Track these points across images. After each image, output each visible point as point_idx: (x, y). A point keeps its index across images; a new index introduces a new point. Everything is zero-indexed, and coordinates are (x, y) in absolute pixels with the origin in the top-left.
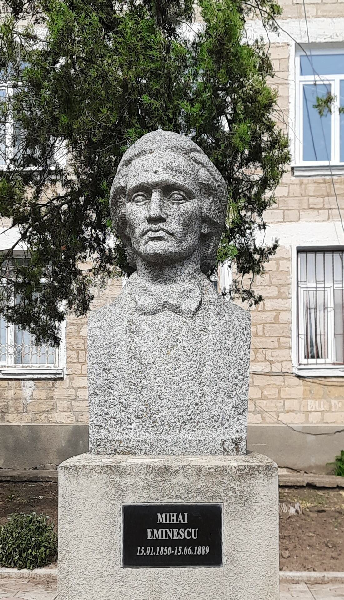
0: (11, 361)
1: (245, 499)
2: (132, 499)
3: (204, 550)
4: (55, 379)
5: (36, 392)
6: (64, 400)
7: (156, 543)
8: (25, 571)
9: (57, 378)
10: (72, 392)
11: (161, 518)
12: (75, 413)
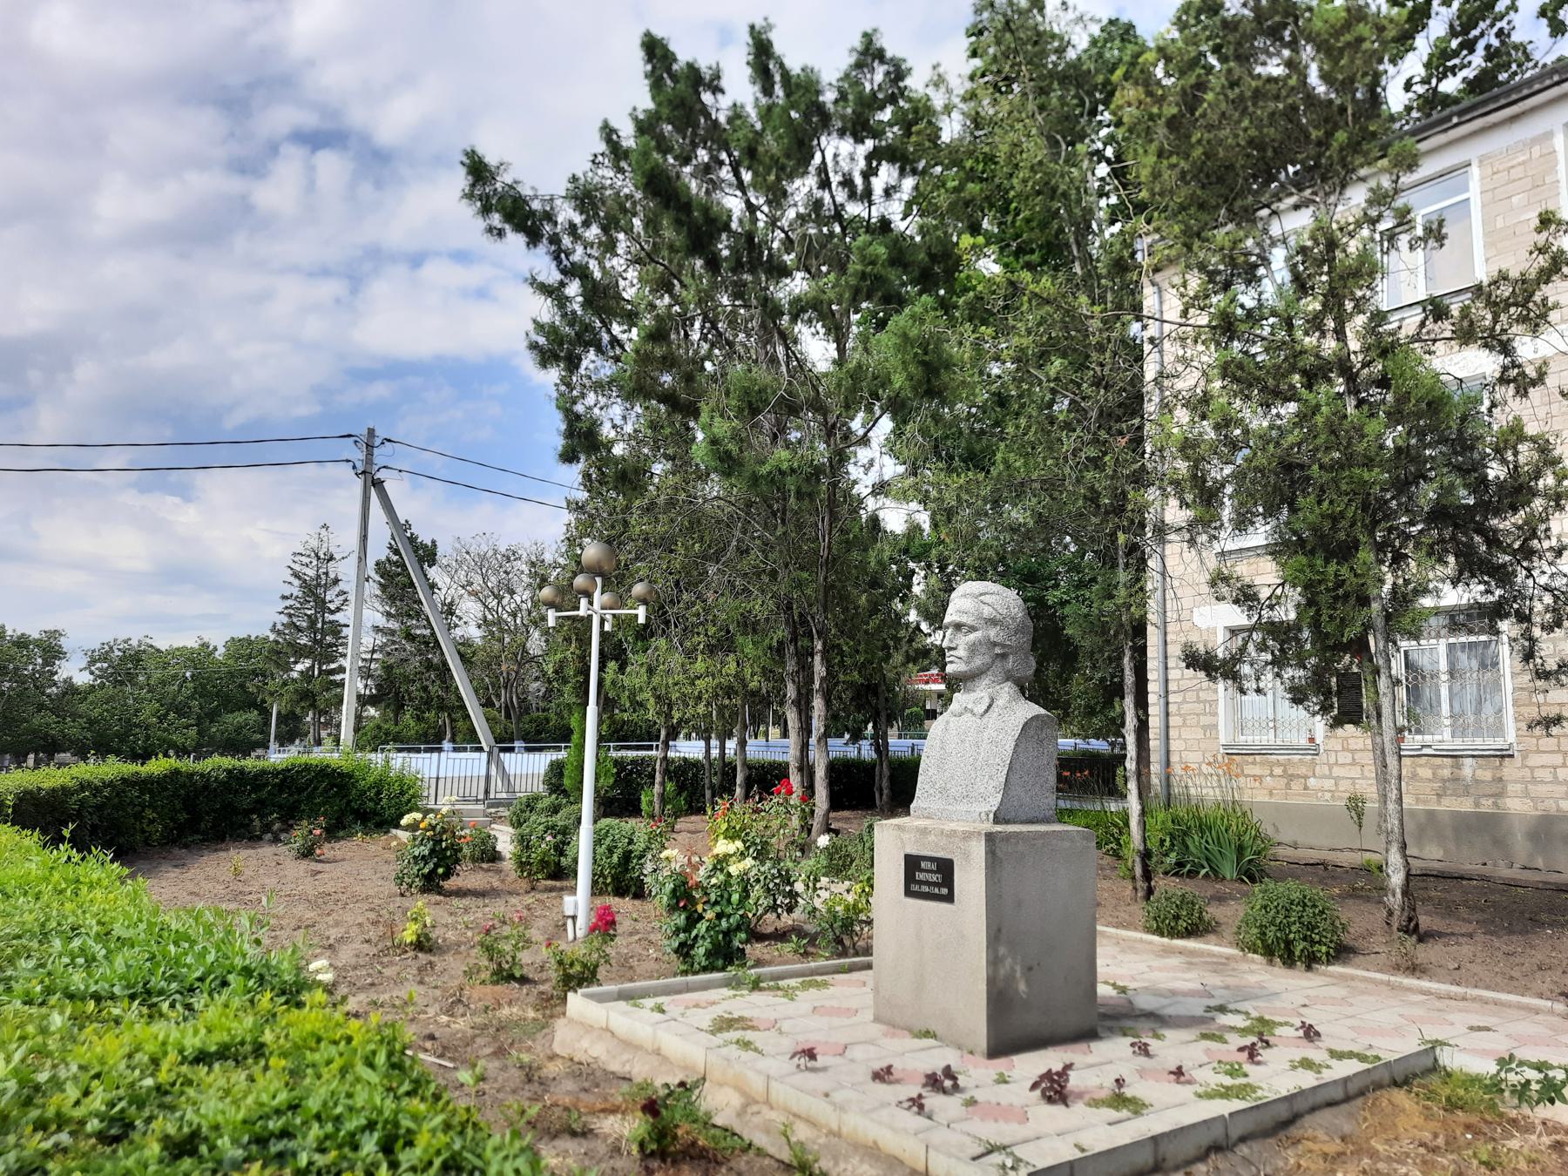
0: (1447, 735)
1: (967, 856)
2: (909, 851)
3: (945, 891)
4: (1503, 757)
5: (1479, 772)
6: (1516, 782)
7: (921, 883)
8: (1166, 940)
9: (1504, 756)
10: (1527, 772)
11: (923, 865)
12: (1532, 799)
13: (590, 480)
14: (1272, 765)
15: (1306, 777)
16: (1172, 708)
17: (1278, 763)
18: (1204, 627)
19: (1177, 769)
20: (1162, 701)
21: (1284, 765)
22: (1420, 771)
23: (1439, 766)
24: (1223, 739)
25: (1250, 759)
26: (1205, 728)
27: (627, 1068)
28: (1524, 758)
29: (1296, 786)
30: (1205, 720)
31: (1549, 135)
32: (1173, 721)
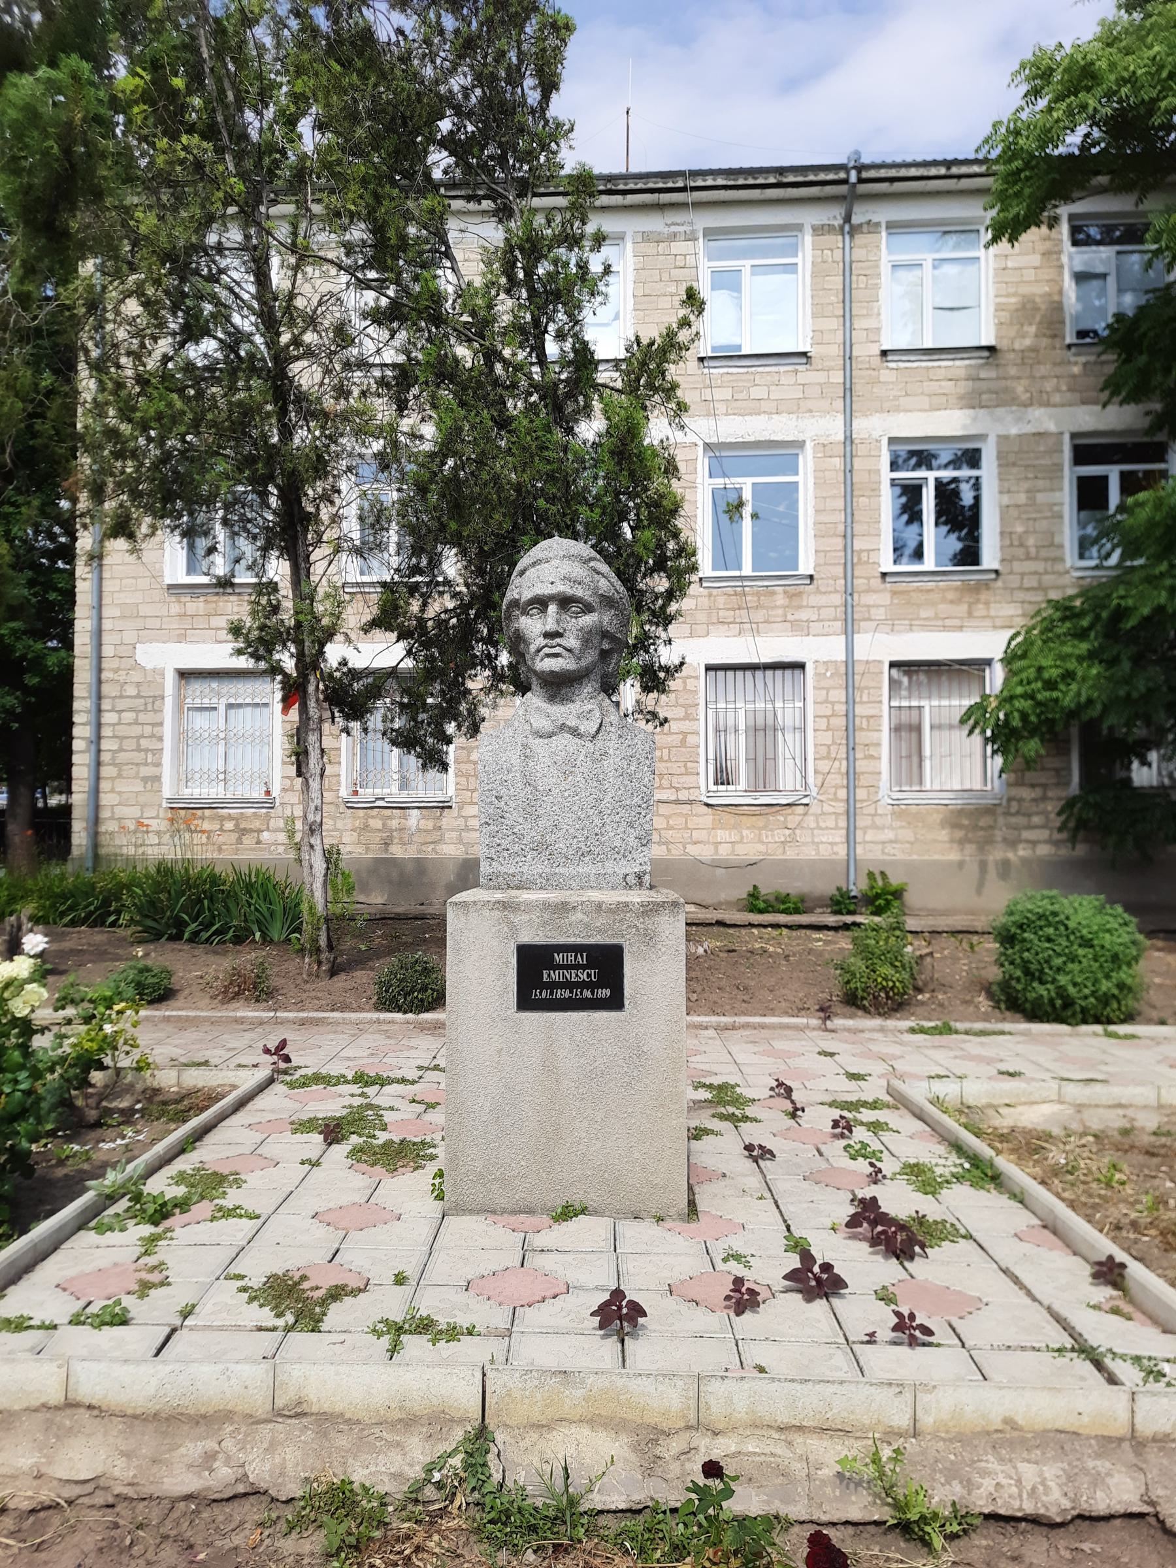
0: (395, 788)
2: (526, 938)
3: (604, 993)
5: (422, 822)
7: (553, 985)
9: (445, 807)
10: (461, 821)
11: (558, 958)
12: (464, 844)
13: (540, 73)
14: (223, 819)
15: (259, 831)
16: (105, 757)
17: (230, 818)
18: (149, 666)
19: (108, 826)
20: (93, 748)
21: (237, 820)
22: (372, 822)
23: (389, 818)
24: (167, 791)
25: (199, 812)
26: (145, 780)
27: (1017, 1504)
28: (461, 809)
29: (248, 840)
30: (146, 771)
31: (799, 228)
32: (105, 771)
